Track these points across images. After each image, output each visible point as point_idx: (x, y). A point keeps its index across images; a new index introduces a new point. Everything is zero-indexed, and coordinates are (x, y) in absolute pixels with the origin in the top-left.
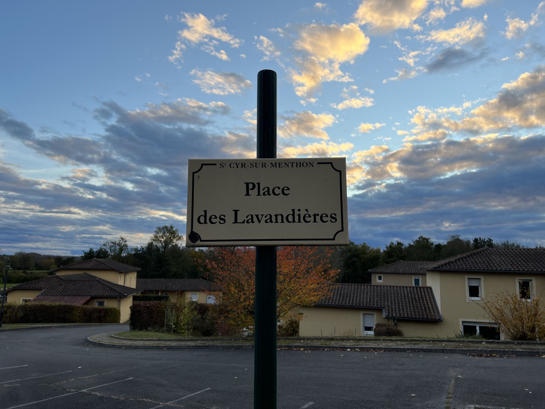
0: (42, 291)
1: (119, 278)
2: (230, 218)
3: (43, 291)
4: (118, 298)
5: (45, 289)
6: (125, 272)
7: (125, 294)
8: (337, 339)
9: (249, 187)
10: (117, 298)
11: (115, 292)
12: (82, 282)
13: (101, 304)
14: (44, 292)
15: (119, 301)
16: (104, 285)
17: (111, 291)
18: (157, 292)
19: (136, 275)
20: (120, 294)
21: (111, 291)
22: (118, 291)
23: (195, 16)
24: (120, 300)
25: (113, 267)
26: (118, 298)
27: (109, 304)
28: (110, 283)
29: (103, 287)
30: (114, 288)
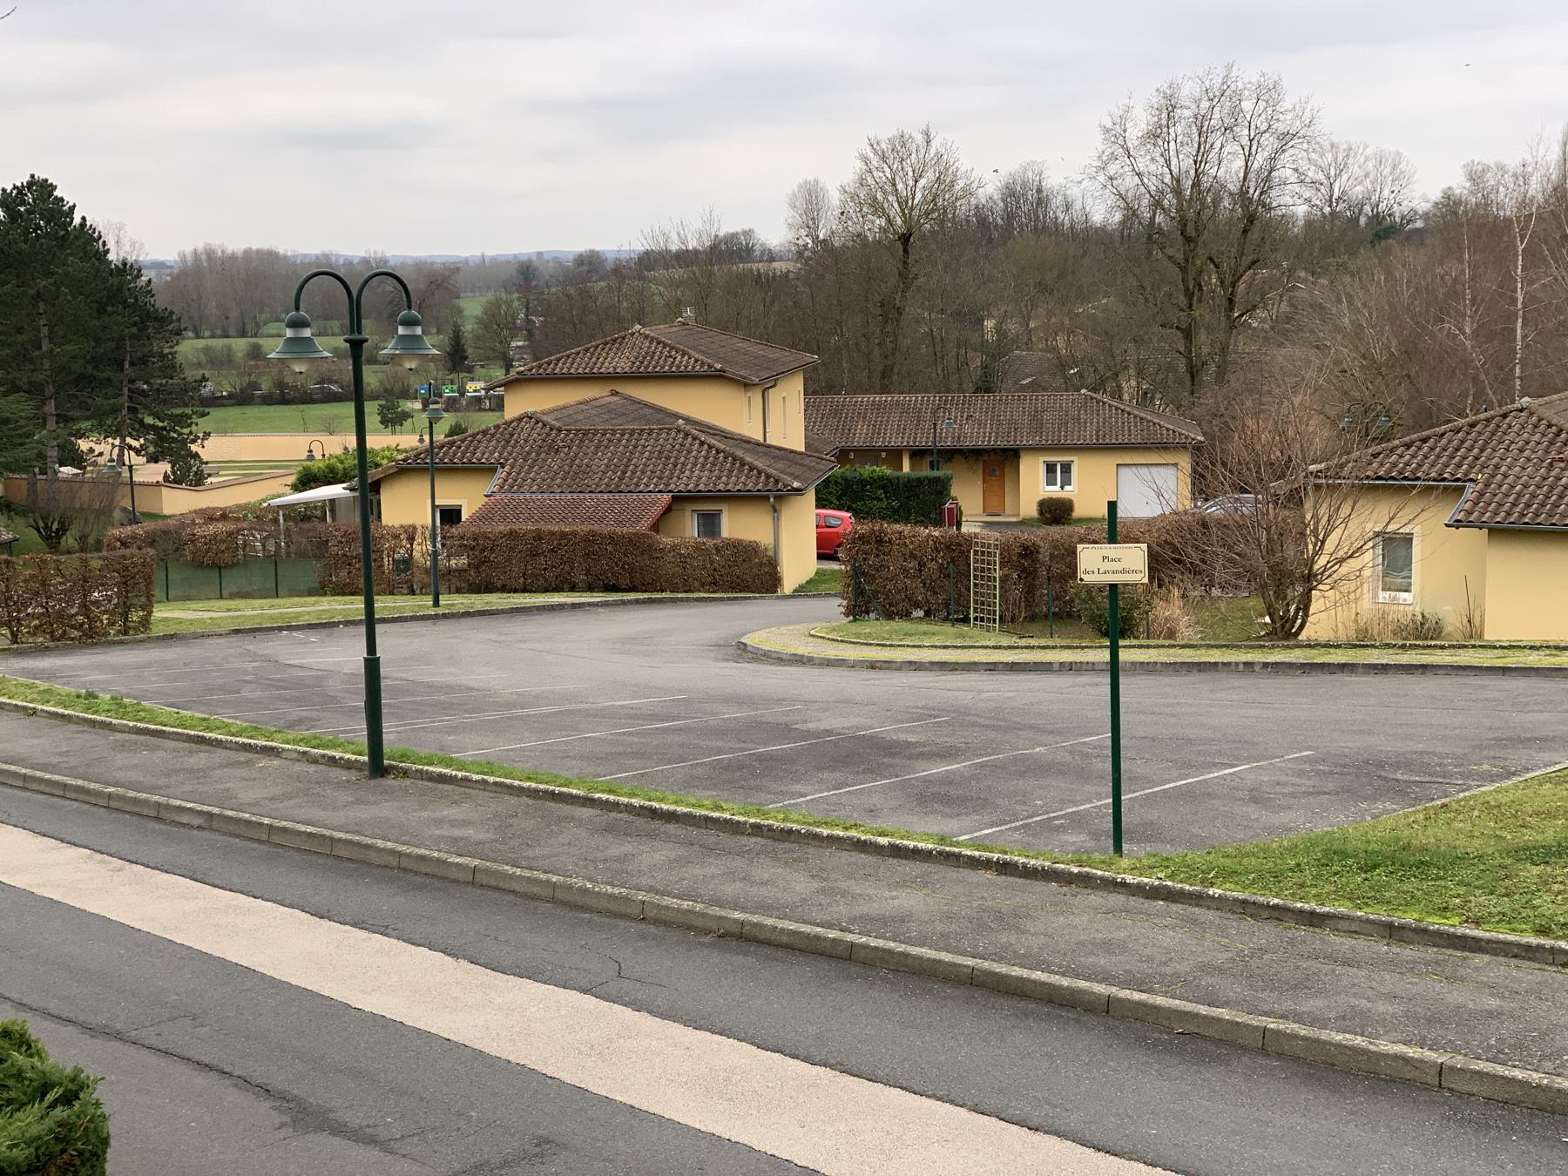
0: (497, 475)
1: (746, 415)
2: (1096, 572)
3: (501, 474)
4: (772, 500)
5: (507, 468)
6: (758, 382)
7: (796, 484)
8: (780, 659)
9: (1104, 558)
10: (768, 498)
11: (758, 478)
12: (627, 436)
13: (710, 523)
14: (506, 481)
15: (775, 510)
16: (710, 447)
17: (741, 471)
18: (895, 455)
19: (801, 388)
20: (777, 482)
21: (741, 471)
22: (770, 470)
23: (960, 184)
24: (777, 507)
25: (719, 366)
26: (772, 500)
27: (740, 526)
28: (725, 435)
29: (706, 458)
30: (748, 459)
